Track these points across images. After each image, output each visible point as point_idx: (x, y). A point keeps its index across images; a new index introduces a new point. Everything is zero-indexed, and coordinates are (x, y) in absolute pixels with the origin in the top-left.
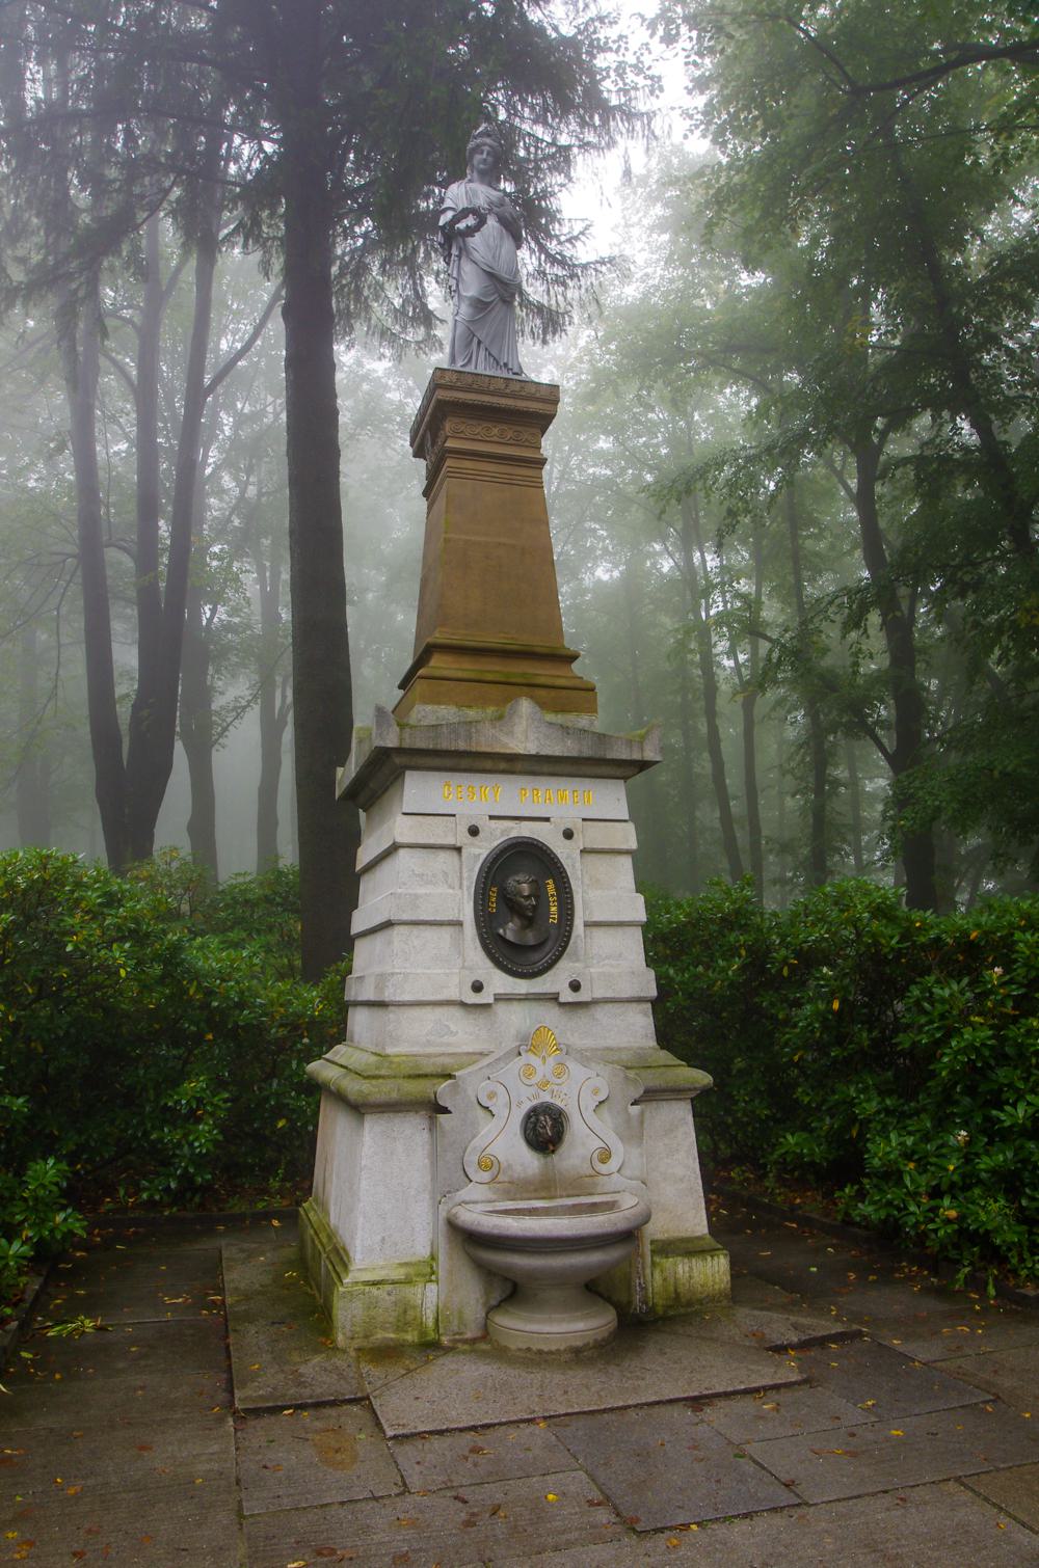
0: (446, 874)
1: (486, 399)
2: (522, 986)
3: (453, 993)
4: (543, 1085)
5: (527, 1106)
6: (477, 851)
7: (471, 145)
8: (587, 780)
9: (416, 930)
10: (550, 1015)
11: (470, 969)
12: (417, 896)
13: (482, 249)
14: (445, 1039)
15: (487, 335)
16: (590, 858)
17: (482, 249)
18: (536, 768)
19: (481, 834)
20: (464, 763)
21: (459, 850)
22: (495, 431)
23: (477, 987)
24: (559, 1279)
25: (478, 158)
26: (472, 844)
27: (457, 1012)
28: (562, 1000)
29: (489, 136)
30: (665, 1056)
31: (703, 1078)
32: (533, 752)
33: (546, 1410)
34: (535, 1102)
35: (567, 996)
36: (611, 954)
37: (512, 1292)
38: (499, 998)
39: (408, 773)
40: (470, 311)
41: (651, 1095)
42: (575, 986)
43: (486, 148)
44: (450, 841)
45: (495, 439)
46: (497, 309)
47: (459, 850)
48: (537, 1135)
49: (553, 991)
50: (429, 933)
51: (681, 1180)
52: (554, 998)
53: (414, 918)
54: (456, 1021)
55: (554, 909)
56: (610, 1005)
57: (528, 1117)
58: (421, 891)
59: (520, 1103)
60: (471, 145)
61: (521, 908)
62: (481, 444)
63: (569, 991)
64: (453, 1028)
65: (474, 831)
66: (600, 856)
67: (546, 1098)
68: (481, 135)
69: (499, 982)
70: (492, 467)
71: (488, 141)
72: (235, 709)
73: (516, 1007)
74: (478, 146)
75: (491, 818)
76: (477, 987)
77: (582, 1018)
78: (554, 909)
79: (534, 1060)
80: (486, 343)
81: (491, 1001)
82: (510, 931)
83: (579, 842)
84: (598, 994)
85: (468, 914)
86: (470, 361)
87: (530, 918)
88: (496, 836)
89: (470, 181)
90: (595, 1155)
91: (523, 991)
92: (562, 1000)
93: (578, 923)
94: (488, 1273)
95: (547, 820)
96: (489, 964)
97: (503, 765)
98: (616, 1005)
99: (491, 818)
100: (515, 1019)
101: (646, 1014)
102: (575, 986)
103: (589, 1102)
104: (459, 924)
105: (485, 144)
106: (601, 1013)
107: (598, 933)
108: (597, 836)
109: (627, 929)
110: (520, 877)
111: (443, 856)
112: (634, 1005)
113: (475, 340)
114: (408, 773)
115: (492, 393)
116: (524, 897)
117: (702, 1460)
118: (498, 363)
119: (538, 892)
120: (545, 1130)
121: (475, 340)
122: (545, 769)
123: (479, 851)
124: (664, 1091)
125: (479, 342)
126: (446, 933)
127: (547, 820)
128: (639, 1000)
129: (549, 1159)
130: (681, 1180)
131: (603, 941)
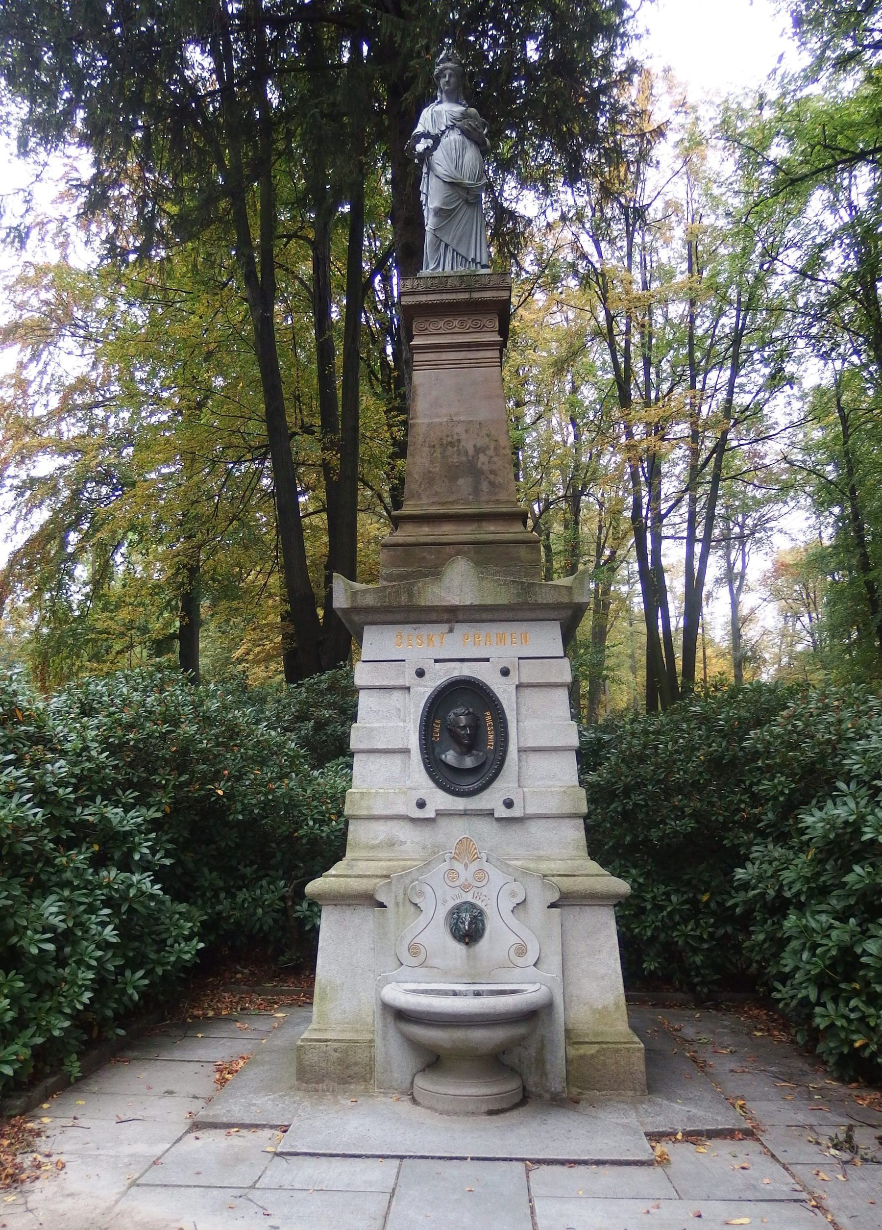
1: (445, 297)
2: (460, 803)
4: (465, 888)
5: (451, 904)
7: (436, 71)
8: (525, 623)
9: (372, 757)
10: (484, 827)
12: (372, 729)
15: (453, 238)
19: (427, 676)
21: (408, 689)
22: (456, 323)
23: (421, 805)
25: (443, 81)
26: (419, 685)
28: (496, 815)
29: (449, 60)
30: (594, 867)
31: (622, 886)
32: (468, 603)
33: (292, 1146)
34: (458, 901)
35: (502, 812)
36: (544, 772)
38: (440, 814)
39: (366, 627)
41: (565, 901)
43: (448, 72)
44: (400, 682)
45: (456, 330)
46: (462, 213)
47: (408, 689)
48: (459, 929)
49: (489, 807)
50: (382, 760)
51: (603, 978)
52: (490, 814)
53: (369, 747)
54: (403, 832)
55: (491, 737)
56: (544, 821)
57: (451, 913)
59: (445, 901)
60: (436, 71)
61: (464, 735)
62: (455, 336)
63: (503, 808)
65: (420, 673)
66: (537, 689)
67: (469, 898)
68: (442, 61)
70: (452, 356)
74: (441, 71)
75: (436, 661)
76: (421, 805)
77: (514, 833)
78: (491, 737)
79: (459, 867)
80: (454, 245)
81: (433, 815)
82: (450, 757)
83: (514, 679)
84: (530, 811)
85: (413, 742)
86: (439, 264)
87: (470, 742)
88: (440, 676)
89: (440, 102)
90: (512, 950)
91: (461, 808)
92: (496, 815)
93: (513, 748)
95: (487, 660)
96: (431, 784)
97: (510, 615)
98: (550, 820)
99: (436, 661)
100: (457, 829)
102: (509, 804)
103: (506, 905)
104: (406, 751)
105: (446, 68)
106: (535, 828)
108: (530, 673)
109: (390, 756)
111: (397, 695)
112: (567, 820)
114: (366, 627)
115: (491, 289)
116: (460, 727)
117: (69, 1195)
118: (466, 260)
119: (477, 726)
120: (468, 928)
122: (485, 616)
123: (424, 690)
125: (447, 246)
126: (397, 759)
127: (487, 660)
129: (472, 949)
130: (603, 978)
131: (537, 765)
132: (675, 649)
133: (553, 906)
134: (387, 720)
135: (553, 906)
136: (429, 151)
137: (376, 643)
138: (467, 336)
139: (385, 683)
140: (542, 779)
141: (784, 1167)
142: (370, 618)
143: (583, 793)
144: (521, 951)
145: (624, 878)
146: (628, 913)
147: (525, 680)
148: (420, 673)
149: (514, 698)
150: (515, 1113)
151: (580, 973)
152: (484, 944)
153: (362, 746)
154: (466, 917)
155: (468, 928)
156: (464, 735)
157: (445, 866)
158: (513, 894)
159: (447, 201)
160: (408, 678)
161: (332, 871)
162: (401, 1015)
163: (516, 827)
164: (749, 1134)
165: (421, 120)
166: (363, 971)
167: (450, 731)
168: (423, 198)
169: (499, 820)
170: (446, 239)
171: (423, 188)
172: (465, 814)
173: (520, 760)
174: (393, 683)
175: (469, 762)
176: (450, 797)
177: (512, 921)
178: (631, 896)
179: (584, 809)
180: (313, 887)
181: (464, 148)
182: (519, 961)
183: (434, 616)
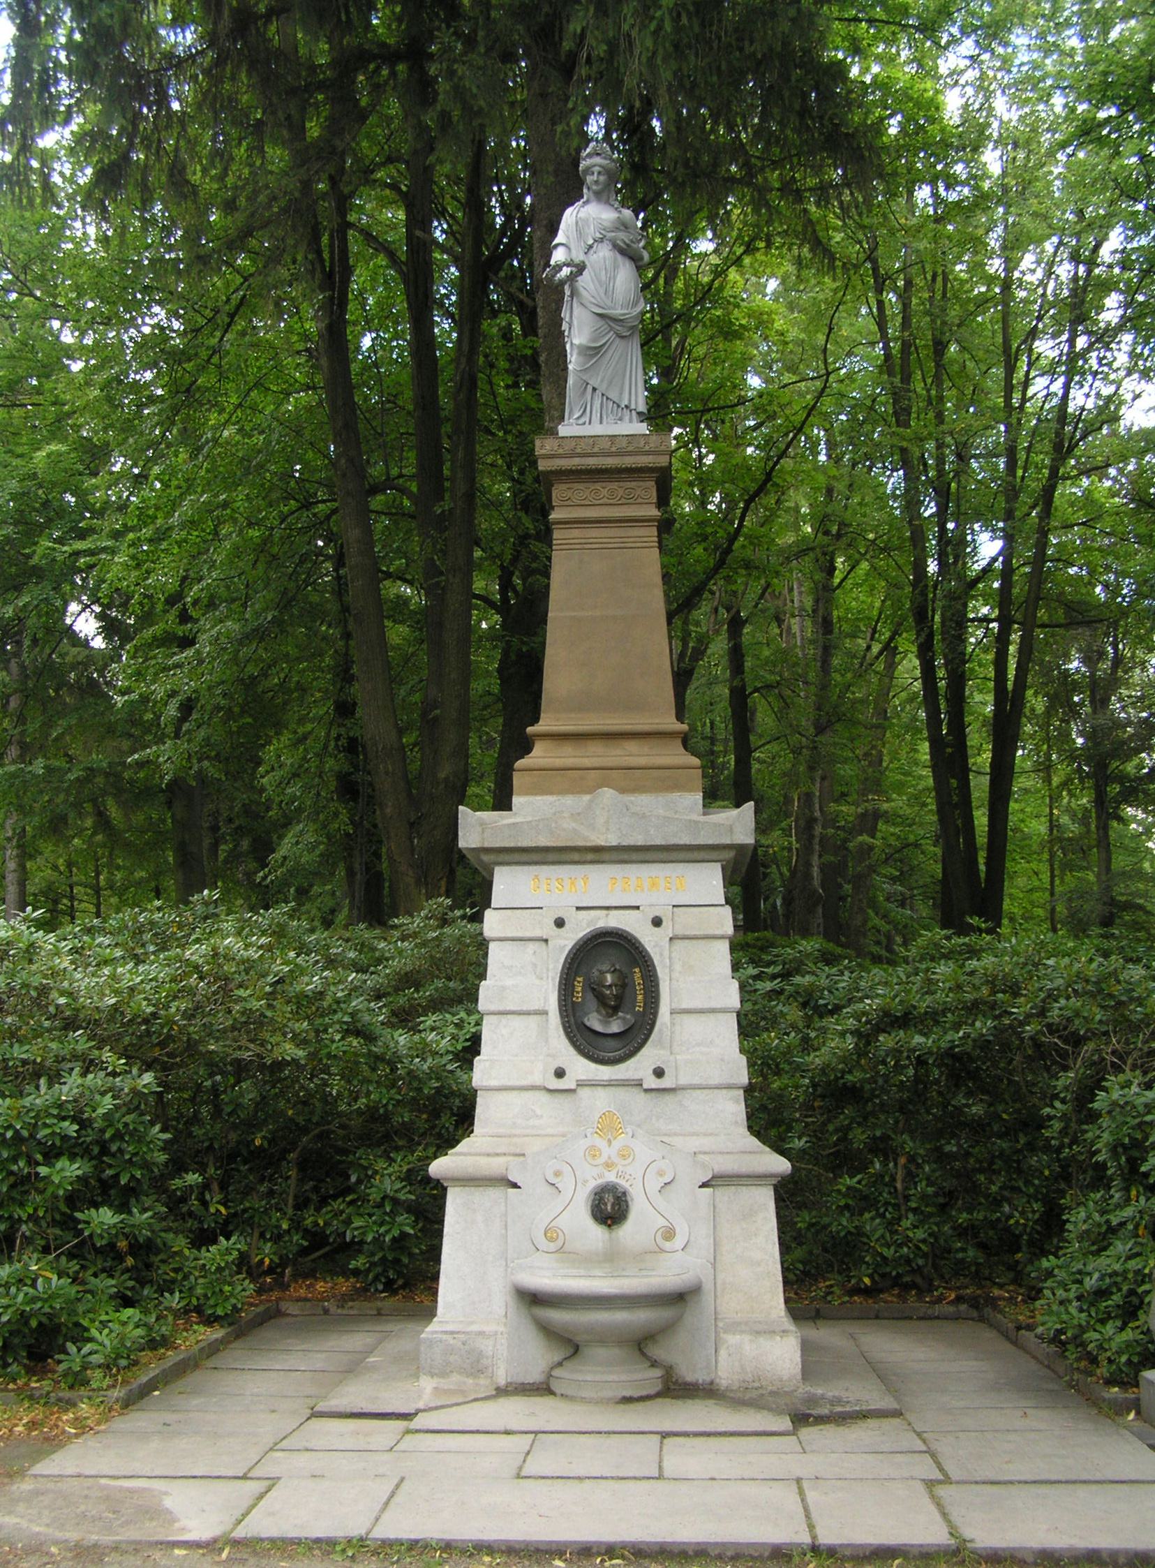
0: (535, 965)
3: (537, 1079)
4: (609, 1165)
5: (592, 1184)
6: (562, 942)
8: (634, 866)
11: (553, 1056)
12: (504, 988)
13: (591, 287)
14: (531, 1122)
16: (679, 944)
17: (591, 287)
18: (626, 857)
19: (567, 926)
20: (551, 857)
21: (546, 941)
22: (604, 492)
23: (560, 1073)
24: (604, 1337)
27: (544, 1097)
31: (781, 1165)
34: (600, 1181)
37: (571, 1346)
38: (581, 1084)
40: (581, 359)
42: (659, 1073)
43: (597, 169)
44: (538, 933)
47: (546, 941)
48: (601, 1211)
50: (516, 1021)
52: (639, 1084)
53: (501, 1008)
58: (509, 982)
59: (586, 1181)
61: (609, 994)
64: (539, 1112)
65: (560, 923)
67: (611, 1177)
68: (589, 156)
69: (581, 1068)
70: (594, 533)
71: (597, 160)
72: (1069, 607)
73: (601, 1092)
75: (578, 908)
76: (560, 1073)
79: (600, 1143)
80: (602, 388)
82: (595, 1022)
84: (683, 1081)
89: (587, 202)
94: (549, 1332)
95: (638, 908)
96: (572, 1051)
97: (590, 856)
99: (578, 908)
100: (600, 1101)
101: (737, 1102)
102: (659, 1073)
103: (654, 1184)
104: (545, 1013)
106: (689, 1099)
107: (536, 1006)
108: (688, 922)
110: (605, 967)
111: (532, 946)
113: (590, 389)
119: (624, 984)
120: (610, 1208)
121: (590, 389)
122: (634, 856)
123: (567, 940)
124: (739, 1176)
125: (594, 389)
126: (533, 1021)
127: (638, 908)
128: (729, 1087)
131: (692, 1028)
132: (977, 832)
133: (704, 1185)
134: (520, 980)
135: (704, 1185)
136: (572, 278)
137: (508, 884)
138: (616, 509)
139: (520, 934)
140: (698, 1045)
141: (919, 1434)
142: (501, 857)
143: (743, 1060)
144: (669, 1234)
145: (782, 1152)
146: (788, 1195)
147: (680, 932)
148: (560, 923)
149: (666, 953)
150: (660, 1400)
151: (732, 1252)
152: (627, 1231)
153: (493, 1008)
154: (609, 1199)
155: (610, 1208)
156: (609, 994)
157: (584, 1143)
158: (661, 1173)
159: (596, 336)
160: (549, 930)
161: (459, 1148)
162: (532, 1299)
163: (668, 1098)
164: (897, 1414)
165: (562, 226)
166: (482, 1261)
167: (593, 990)
168: (565, 326)
169: (647, 1091)
170: (594, 382)
171: (565, 313)
172: (610, 1084)
173: (673, 1024)
174: (528, 934)
175: (615, 1027)
176: (593, 1066)
177: (659, 1201)
178: (792, 1175)
179: (744, 1079)
180: (437, 1167)
181: (616, 267)
182: (667, 1245)
183: (576, 857)
